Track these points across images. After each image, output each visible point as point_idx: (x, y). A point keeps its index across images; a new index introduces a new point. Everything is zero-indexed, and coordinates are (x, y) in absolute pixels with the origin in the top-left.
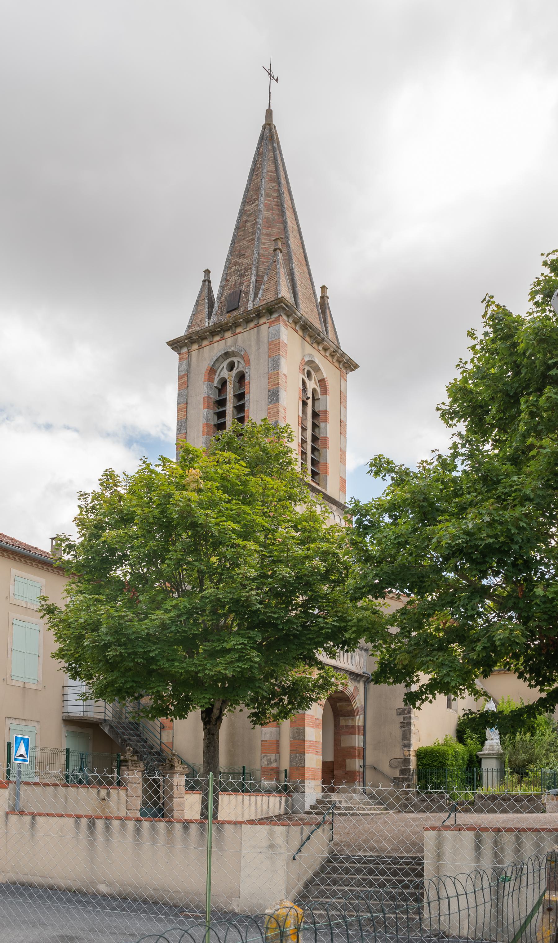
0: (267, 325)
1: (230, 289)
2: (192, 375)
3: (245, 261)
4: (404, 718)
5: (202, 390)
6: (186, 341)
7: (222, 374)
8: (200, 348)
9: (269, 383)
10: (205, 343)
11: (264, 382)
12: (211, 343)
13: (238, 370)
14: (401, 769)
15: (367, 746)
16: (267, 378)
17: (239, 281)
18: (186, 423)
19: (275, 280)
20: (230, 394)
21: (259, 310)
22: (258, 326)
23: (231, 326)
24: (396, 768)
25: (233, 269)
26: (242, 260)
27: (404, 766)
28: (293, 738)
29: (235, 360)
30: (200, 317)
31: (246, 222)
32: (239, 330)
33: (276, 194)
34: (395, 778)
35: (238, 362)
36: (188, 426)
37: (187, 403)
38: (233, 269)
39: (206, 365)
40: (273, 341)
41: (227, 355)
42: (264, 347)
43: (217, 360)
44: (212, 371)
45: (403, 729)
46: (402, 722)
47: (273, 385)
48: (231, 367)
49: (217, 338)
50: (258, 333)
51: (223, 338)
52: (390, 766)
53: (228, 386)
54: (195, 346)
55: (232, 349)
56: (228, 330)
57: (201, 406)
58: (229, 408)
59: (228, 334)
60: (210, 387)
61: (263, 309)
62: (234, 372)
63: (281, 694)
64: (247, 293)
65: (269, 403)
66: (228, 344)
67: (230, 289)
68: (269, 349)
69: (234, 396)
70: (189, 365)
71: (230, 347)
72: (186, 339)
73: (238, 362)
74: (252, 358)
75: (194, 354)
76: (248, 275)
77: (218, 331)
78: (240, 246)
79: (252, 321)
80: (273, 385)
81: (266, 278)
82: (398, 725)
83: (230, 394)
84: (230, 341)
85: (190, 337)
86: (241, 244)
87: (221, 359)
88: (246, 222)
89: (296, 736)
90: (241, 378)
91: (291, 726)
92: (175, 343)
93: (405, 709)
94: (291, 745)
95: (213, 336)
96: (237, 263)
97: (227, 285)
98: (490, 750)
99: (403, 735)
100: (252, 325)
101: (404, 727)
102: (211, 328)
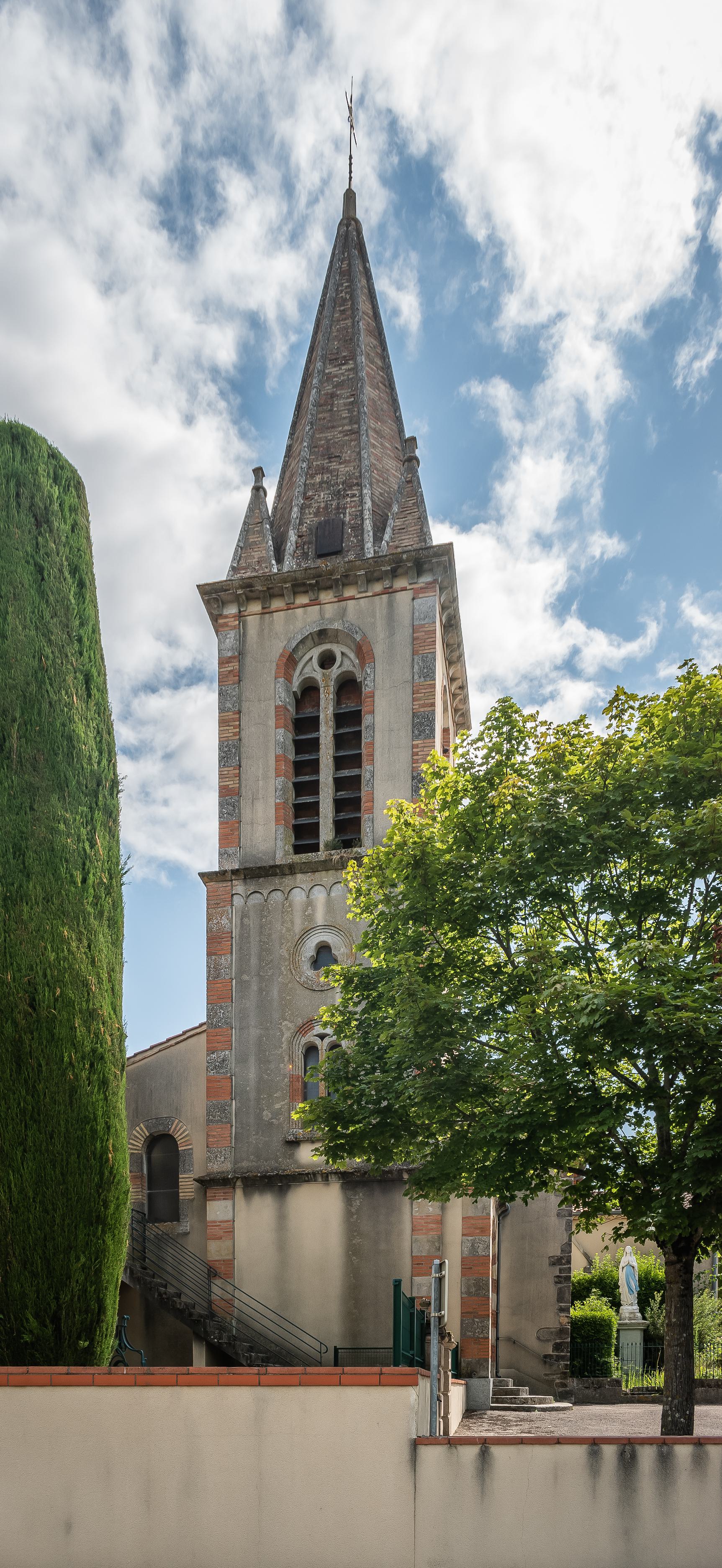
0: (408, 595)
1: (316, 514)
2: (249, 660)
3: (343, 469)
4: (561, 1271)
5: (270, 695)
6: (240, 592)
7: (306, 670)
8: (266, 612)
9: (414, 700)
10: (277, 604)
11: (405, 695)
12: (290, 607)
13: (344, 669)
14: (556, 1344)
15: (502, 1311)
16: (409, 691)
17: (334, 503)
18: (238, 748)
19: (416, 515)
20: (327, 710)
21: (401, 561)
22: (389, 591)
23: (337, 580)
24: (548, 1341)
25: (318, 479)
26: (334, 465)
27: (561, 1338)
28: (468, 1293)
29: (337, 649)
30: (256, 555)
31: (333, 396)
32: (349, 592)
33: (379, 363)
34: (546, 1356)
35: (343, 654)
36: (243, 756)
37: (239, 712)
38: (318, 479)
39: (278, 648)
40: (423, 626)
41: (322, 635)
42: (404, 635)
43: (302, 641)
44: (290, 661)
45: (559, 1286)
46: (558, 1277)
47: (424, 706)
48: (327, 661)
49: (303, 600)
50: (391, 605)
51: (315, 602)
52: (538, 1338)
53: (322, 696)
54: (255, 607)
55: (336, 625)
56: (330, 588)
57: (272, 722)
58: (326, 733)
59: (326, 596)
60: (287, 690)
61: (408, 560)
62: (335, 671)
63: (667, 1206)
64: (359, 529)
65: (415, 737)
66: (327, 616)
67: (316, 514)
68: (414, 639)
69: (334, 714)
70: (242, 638)
71: (331, 621)
72: (242, 587)
73: (343, 654)
74: (379, 649)
75: (252, 622)
76: (354, 496)
77: (307, 585)
78: (328, 441)
79: (378, 579)
80: (424, 706)
81: (395, 509)
82: (552, 1280)
83: (327, 710)
84: (330, 610)
85: (250, 586)
86: (329, 435)
87: (309, 643)
88: (333, 396)
89: (473, 1290)
90: (348, 686)
91: (463, 1275)
92: (216, 591)
93: (562, 1258)
94: (463, 1304)
95: (295, 594)
96: (322, 470)
97: (309, 506)
98: (630, 1319)
99: (558, 1294)
100: (378, 587)
101: (560, 1282)
102: (298, 575)
